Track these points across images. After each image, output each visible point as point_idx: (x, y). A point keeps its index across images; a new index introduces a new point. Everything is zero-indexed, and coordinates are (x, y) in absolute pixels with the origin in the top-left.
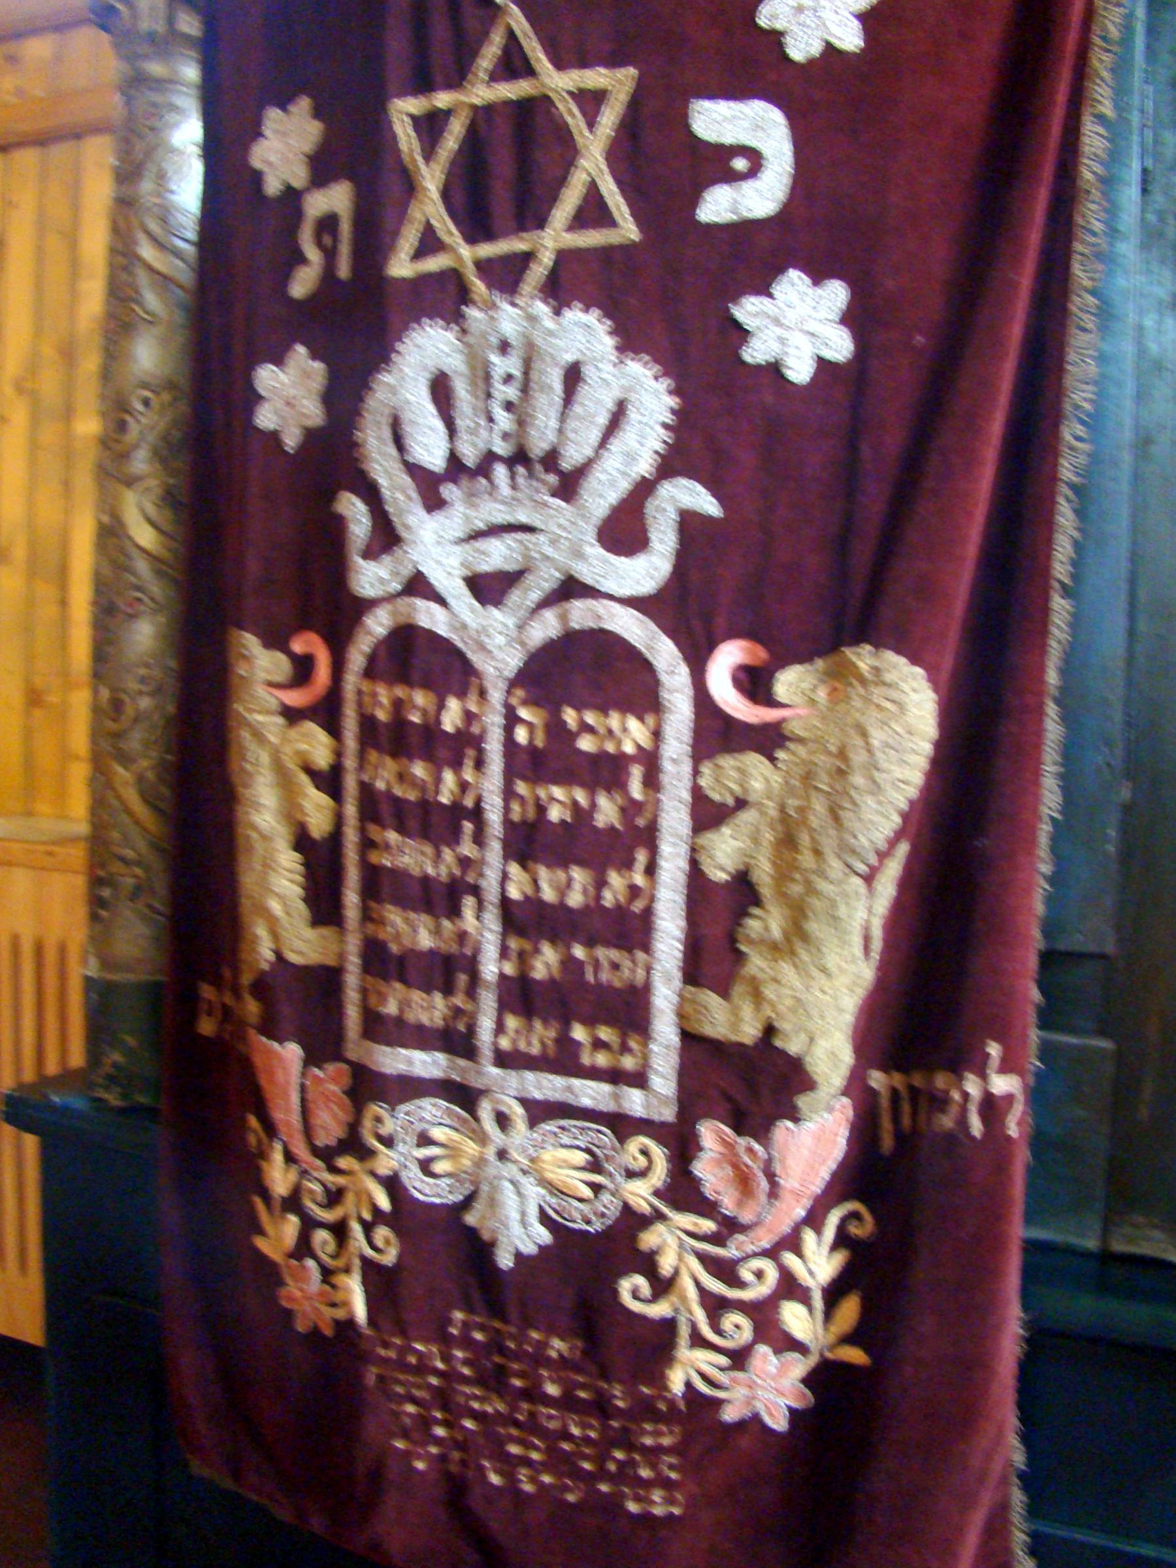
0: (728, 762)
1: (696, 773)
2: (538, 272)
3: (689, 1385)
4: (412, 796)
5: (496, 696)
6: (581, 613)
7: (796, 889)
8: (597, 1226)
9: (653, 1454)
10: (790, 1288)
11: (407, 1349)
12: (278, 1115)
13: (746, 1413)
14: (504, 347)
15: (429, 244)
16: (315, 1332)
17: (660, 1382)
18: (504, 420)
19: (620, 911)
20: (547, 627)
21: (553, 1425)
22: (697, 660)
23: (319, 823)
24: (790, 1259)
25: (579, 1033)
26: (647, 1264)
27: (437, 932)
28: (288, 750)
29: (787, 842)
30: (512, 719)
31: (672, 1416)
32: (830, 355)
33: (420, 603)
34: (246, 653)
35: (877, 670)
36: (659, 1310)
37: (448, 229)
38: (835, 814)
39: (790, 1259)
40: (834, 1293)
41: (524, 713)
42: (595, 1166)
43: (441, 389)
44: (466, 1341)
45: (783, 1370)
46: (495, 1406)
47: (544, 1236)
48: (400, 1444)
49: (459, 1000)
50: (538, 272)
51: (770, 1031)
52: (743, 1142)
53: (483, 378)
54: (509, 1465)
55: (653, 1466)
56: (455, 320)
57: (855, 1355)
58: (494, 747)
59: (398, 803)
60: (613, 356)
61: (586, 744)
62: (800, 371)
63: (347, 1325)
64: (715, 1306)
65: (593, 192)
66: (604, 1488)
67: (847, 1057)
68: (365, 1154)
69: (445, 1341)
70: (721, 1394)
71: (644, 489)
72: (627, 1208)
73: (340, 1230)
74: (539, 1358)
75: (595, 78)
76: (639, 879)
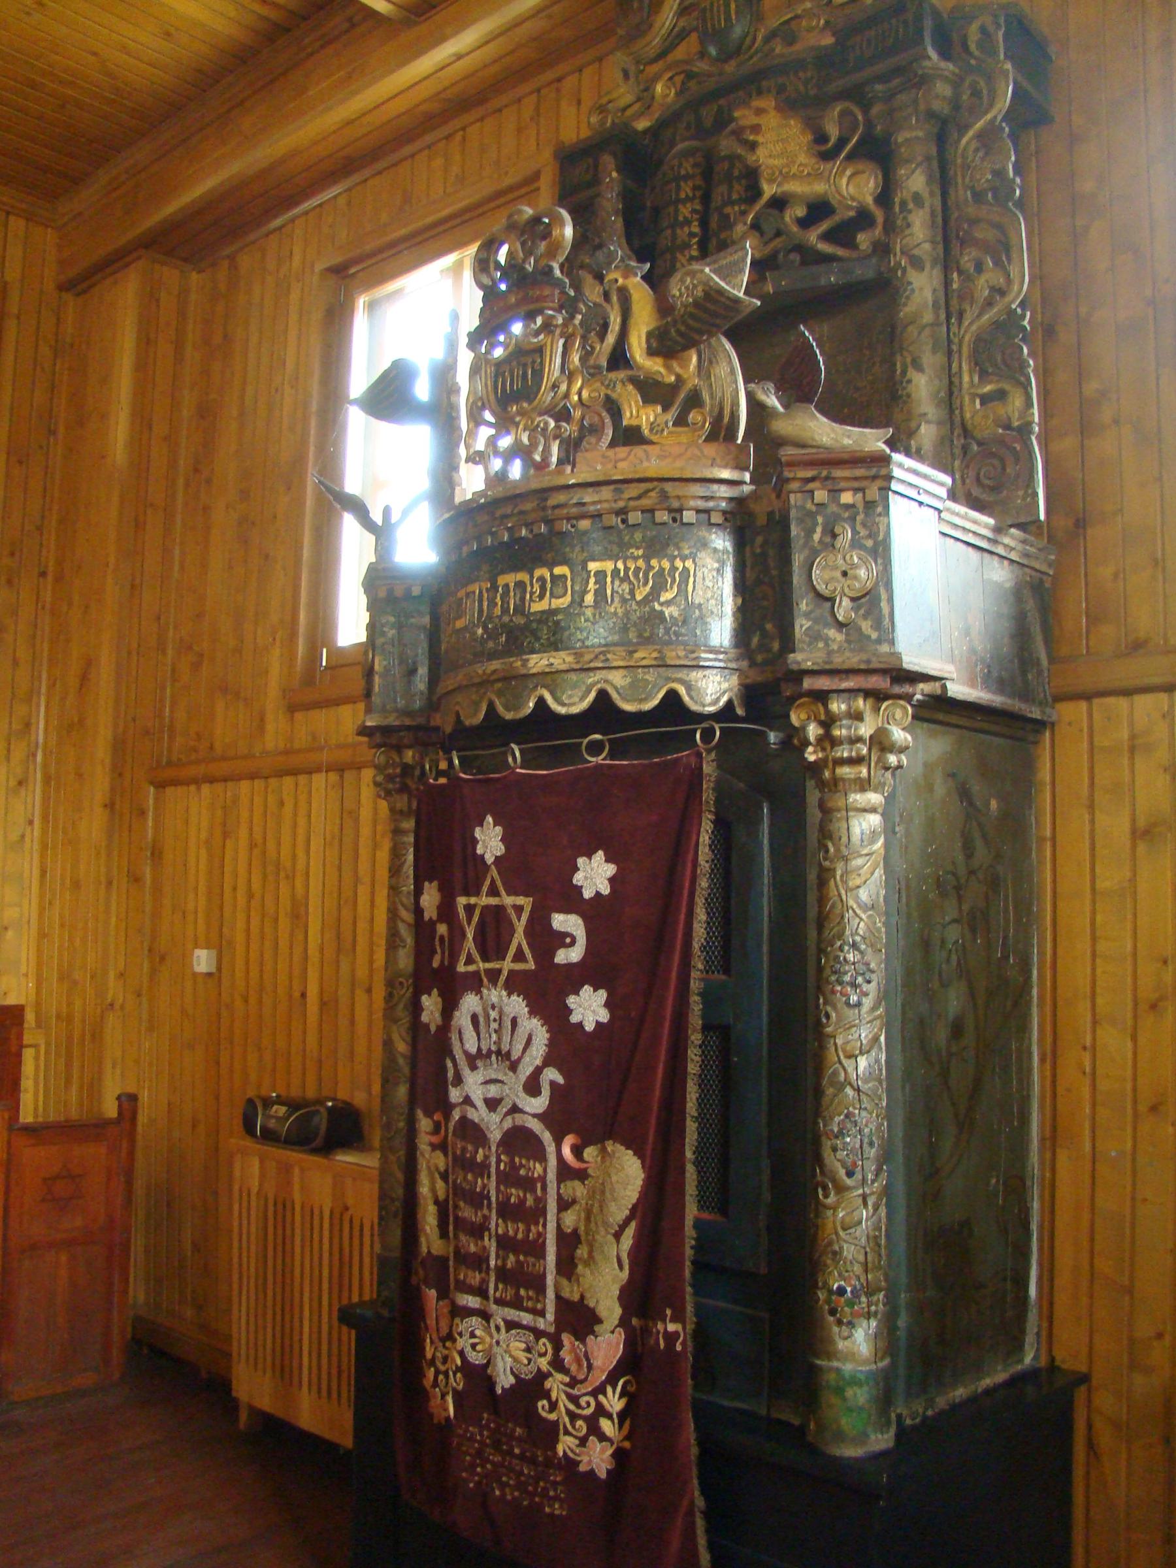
0: (569, 1183)
1: (559, 1188)
2: (503, 978)
3: (564, 1452)
4: (467, 1187)
5: (494, 1149)
6: (519, 1119)
7: (590, 1238)
8: (530, 1376)
9: (555, 1483)
10: (601, 1411)
11: (467, 1430)
12: (428, 1322)
13: (588, 1468)
14: (493, 1007)
15: (470, 961)
16: (440, 1423)
17: (554, 1448)
18: (494, 1037)
19: (535, 1241)
20: (508, 1123)
21: (518, 1468)
22: (559, 1144)
23: (441, 1196)
24: (601, 1397)
25: (522, 1292)
26: (547, 1395)
27: (476, 1245)
28: (432, 1161)
29: (588, 1219)
30: (499, 1161)
31: (559, 1467)
32: (601, 1020)
33: (468, 1108)
34: (1030, 605)
35: (613, 1152)
36: (553, 1417)
37: (476, 955)
38: (601, 1206)
39: (601, 1397)
40: (622, 1415)
41: (503, 1157)
42: (528, 1350)
43: (475, 1019)
44: (489, 1429)
45: (603, 1451)
46: (498, 1459)
47: (512, 1380)
48: (464, 1474)
49: (483, 1275)
50: (503, 978)
51: (582, 1297)
52: (577, 1343)
53: (487, 1016)
54: (503, 1486)
55: (555, 1490)
56: (479, 992)
57: (627, 1445)
58: (493, 1170)
59: (463, 1189)
60: (527, 1016)
61: (522, 1172)
62: (589, 1027)
63: (448, 1418)
64: (573, 1417)
65: (520, 948)
66: (537, 1499)
67: (618, 1311)
68: (454, 1341)
69: (481, 1428)
70: (579, 1459)
71: (538, 1071)
72: (539, 1369)
73: (446, 1374)
74: (511, 1437)
75: (521, 900)
76: (541, 1229)
